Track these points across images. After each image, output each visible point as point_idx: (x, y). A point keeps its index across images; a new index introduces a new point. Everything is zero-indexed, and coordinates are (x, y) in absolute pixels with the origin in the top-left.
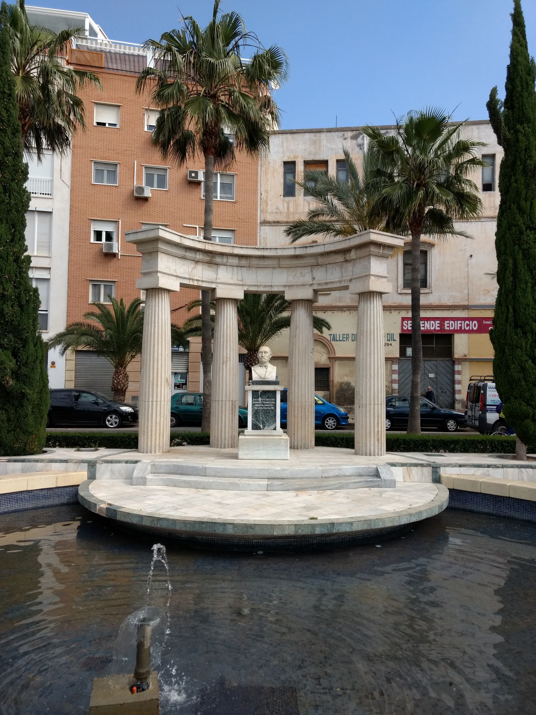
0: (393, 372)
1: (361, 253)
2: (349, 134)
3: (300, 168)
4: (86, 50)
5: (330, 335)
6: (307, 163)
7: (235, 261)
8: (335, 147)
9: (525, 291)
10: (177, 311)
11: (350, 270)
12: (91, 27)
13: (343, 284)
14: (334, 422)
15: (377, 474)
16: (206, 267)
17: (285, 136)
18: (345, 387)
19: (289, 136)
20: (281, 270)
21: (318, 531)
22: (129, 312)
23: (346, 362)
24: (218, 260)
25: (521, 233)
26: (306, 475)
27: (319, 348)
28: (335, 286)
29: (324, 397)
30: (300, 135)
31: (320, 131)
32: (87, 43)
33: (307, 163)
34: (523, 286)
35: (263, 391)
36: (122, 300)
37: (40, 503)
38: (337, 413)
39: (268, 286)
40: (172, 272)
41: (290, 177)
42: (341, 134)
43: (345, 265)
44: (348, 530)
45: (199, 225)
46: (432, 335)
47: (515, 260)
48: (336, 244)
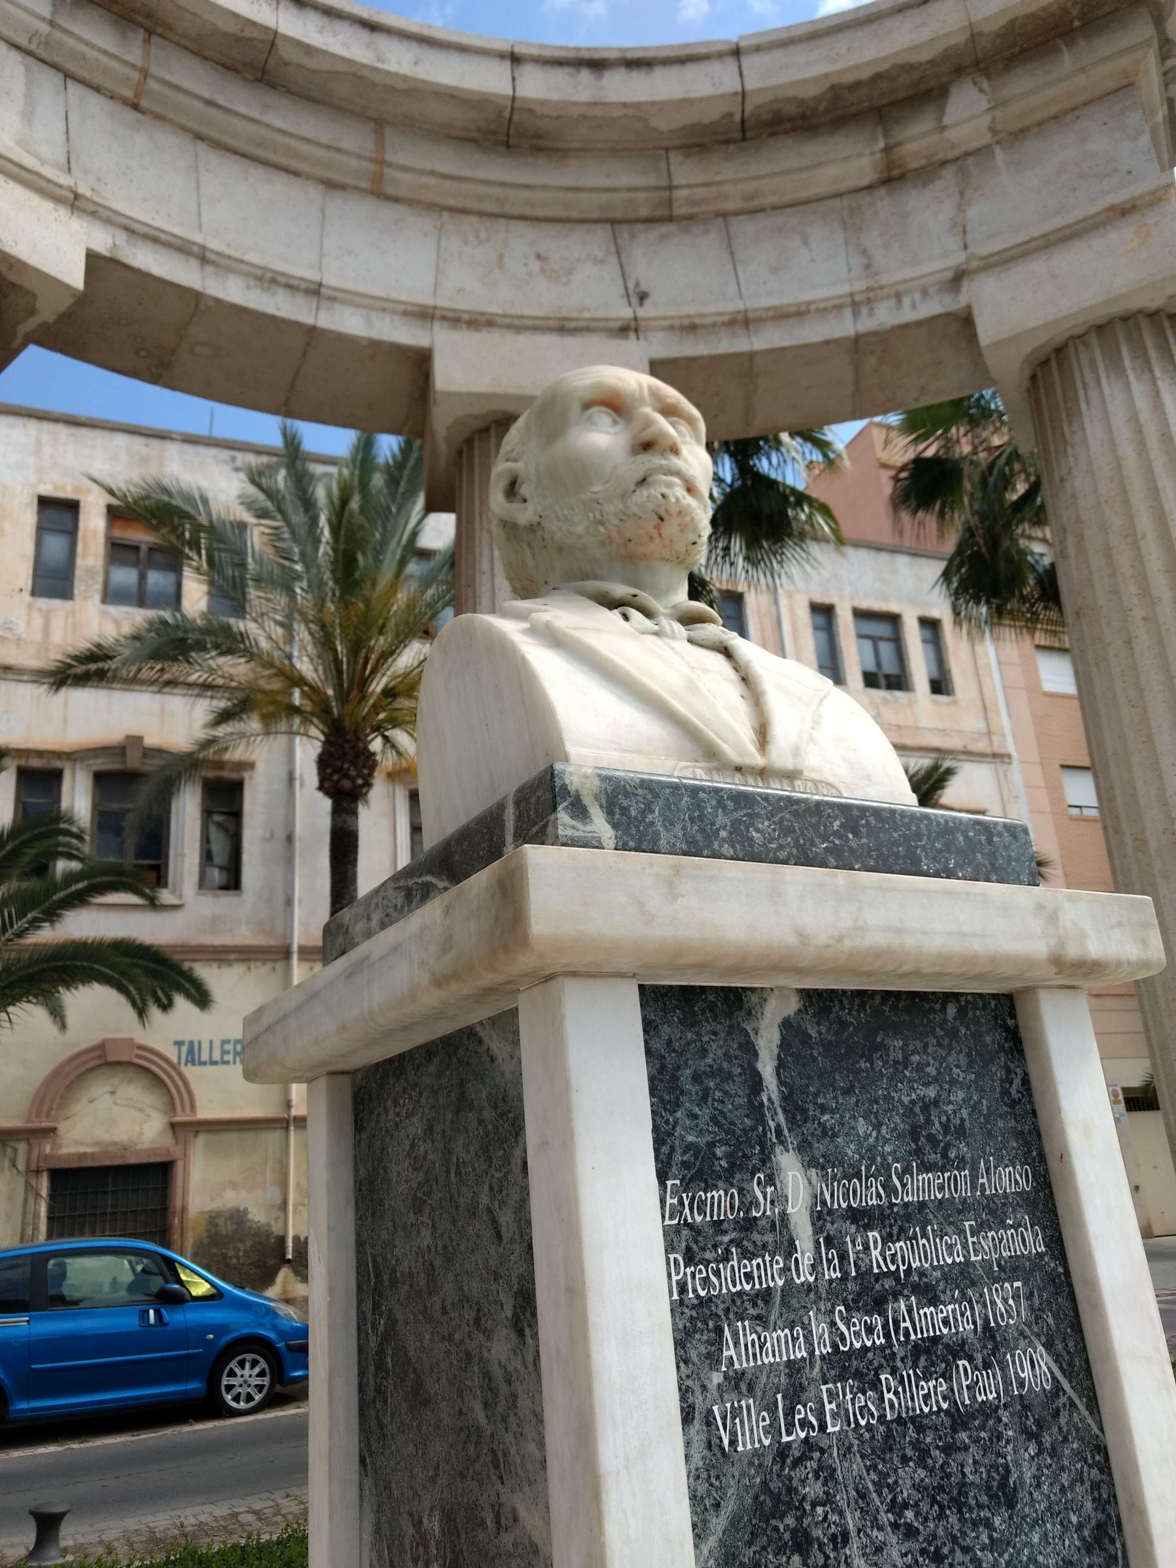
14: (262, 1374)
17: (47, 426)
18: (225, 1228)
19: (63, 431)
20: (389, 212)
23: (233, 1137)
31: (163, 436)
35: (818, 1001)
38: (274, 1328)
39: (291, 286)
41: (56, 545)
42: (226, 454)
48: (840, 44)
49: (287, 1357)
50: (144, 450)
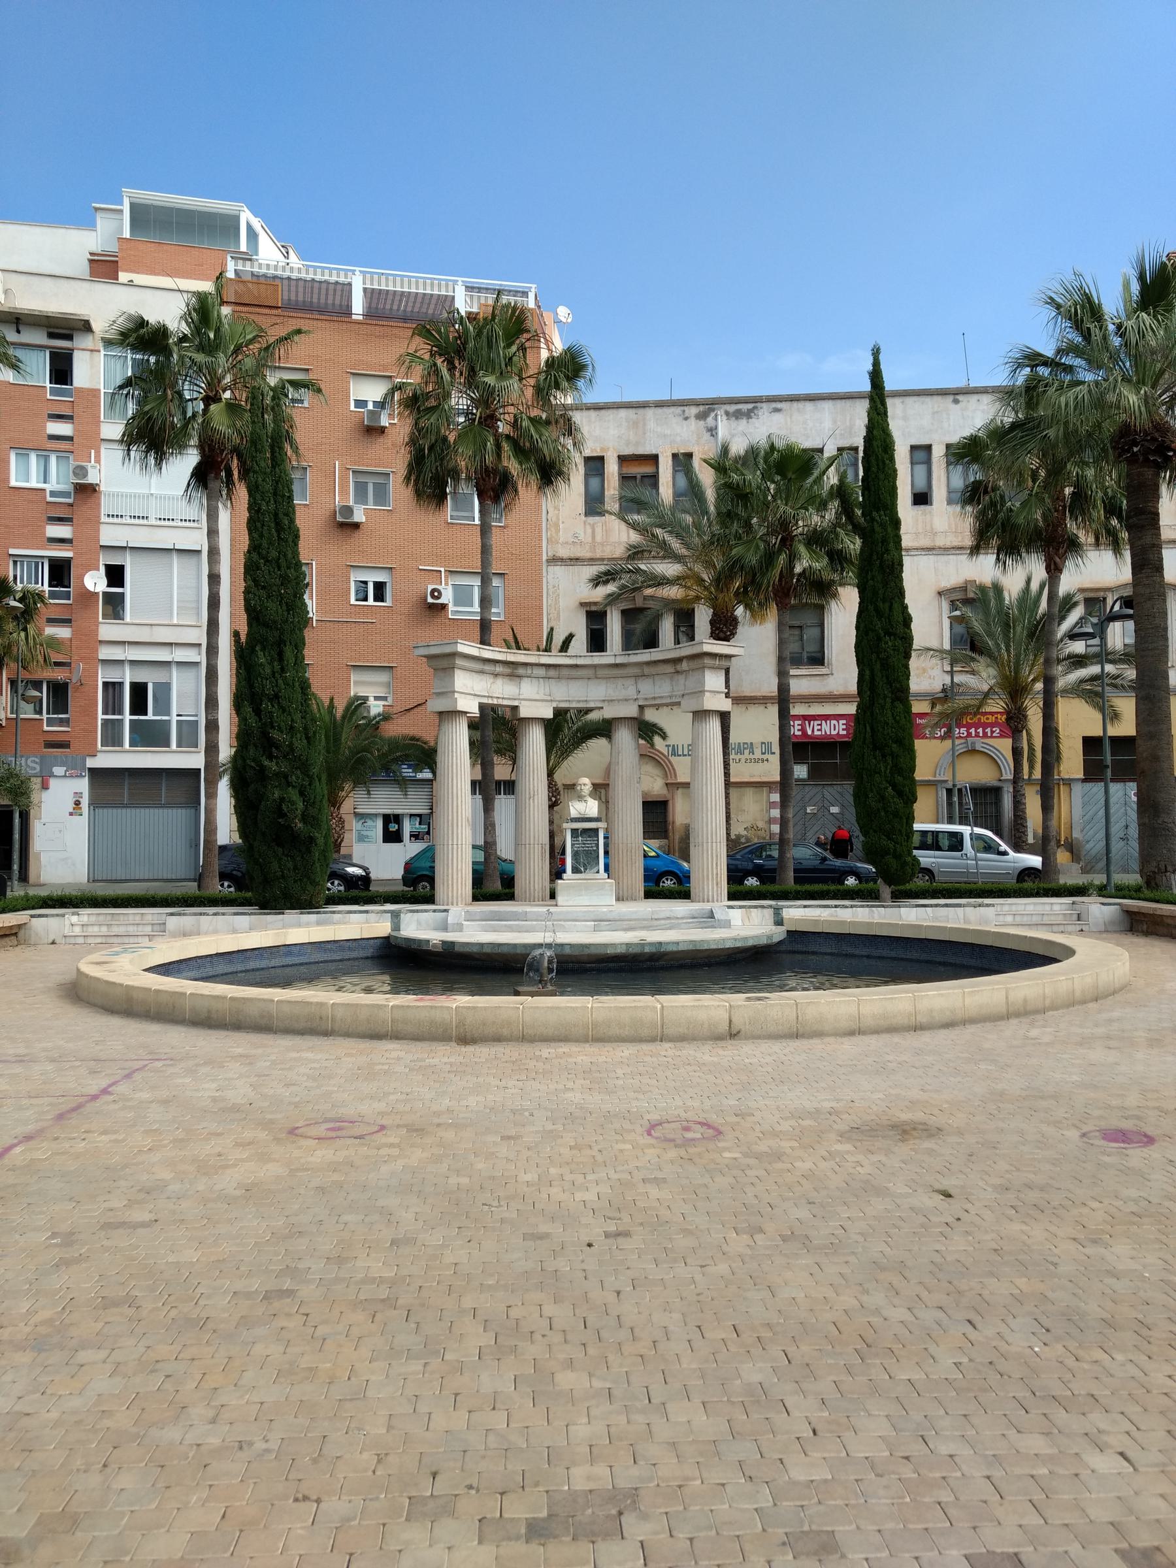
0: (772, 805)
1: (694, 664)
2: (694, 411)
3: (612, 468)
4: (249, 278)
5: (668, 746)
6: (623, 459)
7: (541, 672)
8: (669, 432)
9: (883, 707)
10: (412, 712)
11: (682, 684)
12: (249, 227)
13: (674, 700)
15: (711, 915)
16: (506, 680)
21: (647, 950)
22: (344, 717)
24: (521, 671)
25: (879, 639)
26: (634, 917)
27: (650, 768)
28: (664, 701)
29: (660, 848)
30: (610, 412)
32: (252, 267)
33: (623, 459)
34: (881, 701)
36: (332, 700)
37: (347, 955)
40: (471, 691)
41: (595, 482)
42: (679, 410)
43: (676, 676)
44: (675, 949)
45: (444, 566)
46: (836, 743)
47: (872, 671)
49: (684, 879)
50: (635, 417)
